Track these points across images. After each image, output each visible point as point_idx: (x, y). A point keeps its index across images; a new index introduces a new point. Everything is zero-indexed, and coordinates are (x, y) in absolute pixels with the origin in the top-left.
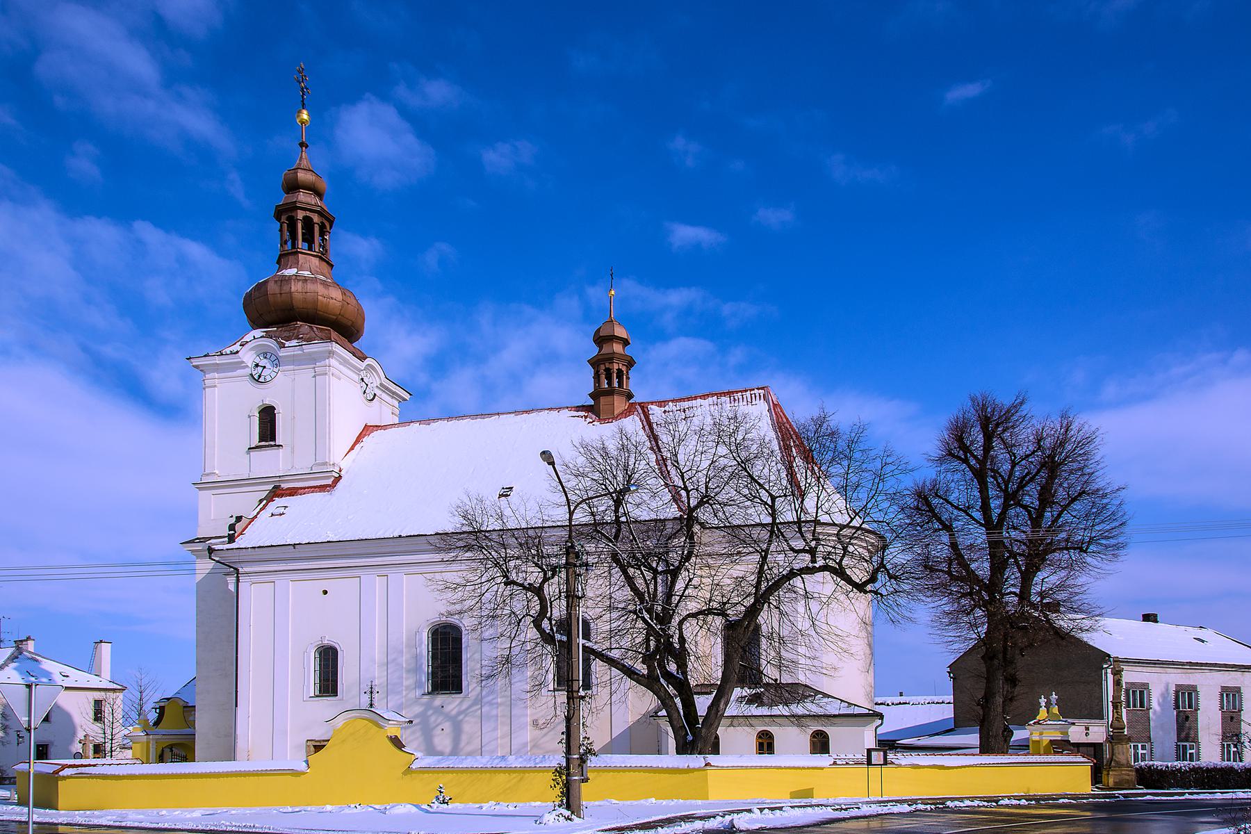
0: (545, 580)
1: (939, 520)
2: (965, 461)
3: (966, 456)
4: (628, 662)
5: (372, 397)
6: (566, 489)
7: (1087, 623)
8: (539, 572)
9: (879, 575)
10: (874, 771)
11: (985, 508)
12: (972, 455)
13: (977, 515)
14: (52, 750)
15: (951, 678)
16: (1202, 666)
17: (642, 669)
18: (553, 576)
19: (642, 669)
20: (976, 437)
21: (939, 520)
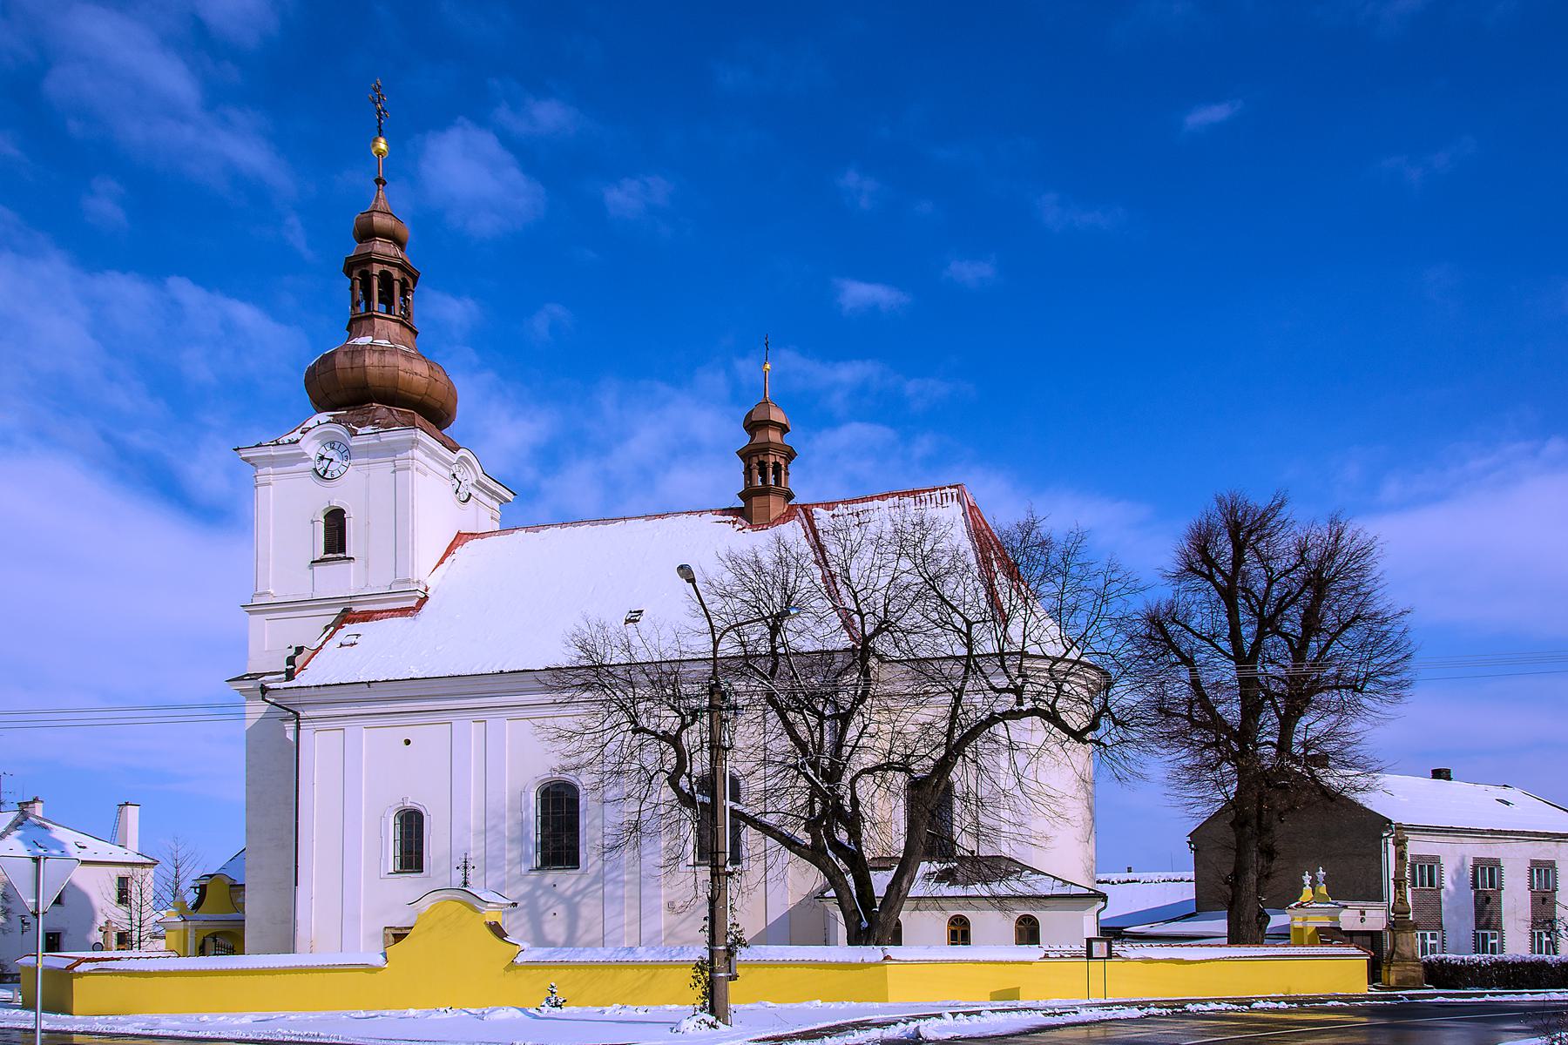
0: (684, 726)
1: (1177, 651)
3: (1211, 572)
4: (787, 830)
5: (466, 497)
6: (710, 613)
8: (676, 717)
11: (1235, 637)
12: (1219, 570)
14: (65, 940)
15: (1192, 849)
17: (805, 838)
18: (693, 722)
19: (805, 838)
20: (1224, 548)
21: (1177, 651)
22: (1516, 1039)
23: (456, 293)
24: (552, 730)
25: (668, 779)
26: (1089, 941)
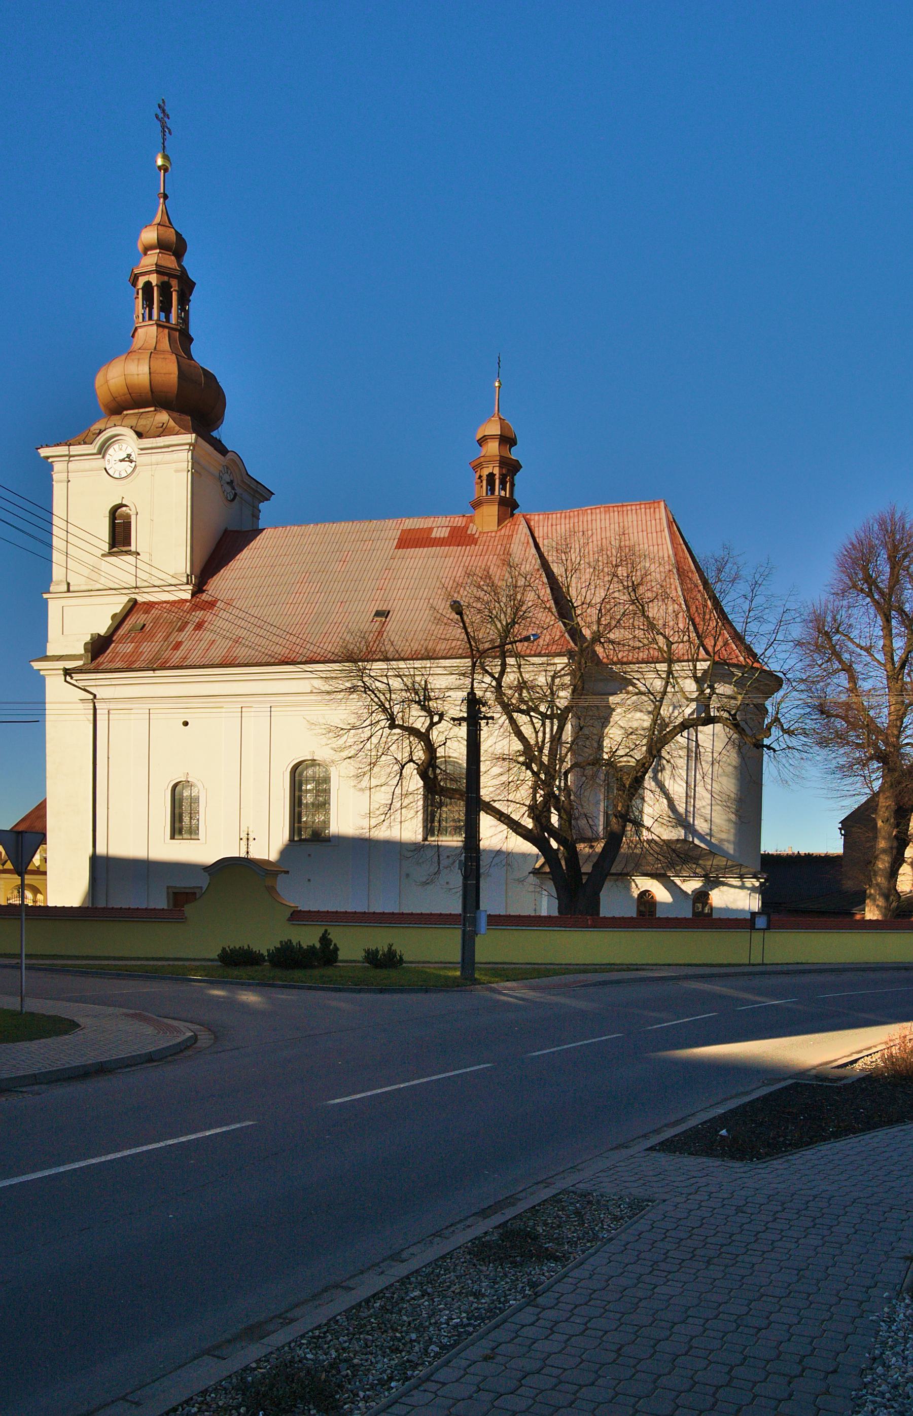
0: (432, 724)
1: (840, 661)
2: (870, 594)
3: (870, 590)
4: (516, 817)
5: (232, 497)
6: (461, 625)
7: (381, 953)
8: (426, 717)
9: (773, 729)
10: (757, 936)
11: (889, 651)
12: (877, 587)
13: (880, 657)
14: (288, 915)
15: (842, 835)
16: (63, 966)
17: (529, 823)
18: (439, 722)
19: (529, 823)
20: (883, 569)
21: (840, 661)
22: (108, 629)
23: (870, 920)
24: (324, 727)
25: (417, 769)
26: (486, 911)
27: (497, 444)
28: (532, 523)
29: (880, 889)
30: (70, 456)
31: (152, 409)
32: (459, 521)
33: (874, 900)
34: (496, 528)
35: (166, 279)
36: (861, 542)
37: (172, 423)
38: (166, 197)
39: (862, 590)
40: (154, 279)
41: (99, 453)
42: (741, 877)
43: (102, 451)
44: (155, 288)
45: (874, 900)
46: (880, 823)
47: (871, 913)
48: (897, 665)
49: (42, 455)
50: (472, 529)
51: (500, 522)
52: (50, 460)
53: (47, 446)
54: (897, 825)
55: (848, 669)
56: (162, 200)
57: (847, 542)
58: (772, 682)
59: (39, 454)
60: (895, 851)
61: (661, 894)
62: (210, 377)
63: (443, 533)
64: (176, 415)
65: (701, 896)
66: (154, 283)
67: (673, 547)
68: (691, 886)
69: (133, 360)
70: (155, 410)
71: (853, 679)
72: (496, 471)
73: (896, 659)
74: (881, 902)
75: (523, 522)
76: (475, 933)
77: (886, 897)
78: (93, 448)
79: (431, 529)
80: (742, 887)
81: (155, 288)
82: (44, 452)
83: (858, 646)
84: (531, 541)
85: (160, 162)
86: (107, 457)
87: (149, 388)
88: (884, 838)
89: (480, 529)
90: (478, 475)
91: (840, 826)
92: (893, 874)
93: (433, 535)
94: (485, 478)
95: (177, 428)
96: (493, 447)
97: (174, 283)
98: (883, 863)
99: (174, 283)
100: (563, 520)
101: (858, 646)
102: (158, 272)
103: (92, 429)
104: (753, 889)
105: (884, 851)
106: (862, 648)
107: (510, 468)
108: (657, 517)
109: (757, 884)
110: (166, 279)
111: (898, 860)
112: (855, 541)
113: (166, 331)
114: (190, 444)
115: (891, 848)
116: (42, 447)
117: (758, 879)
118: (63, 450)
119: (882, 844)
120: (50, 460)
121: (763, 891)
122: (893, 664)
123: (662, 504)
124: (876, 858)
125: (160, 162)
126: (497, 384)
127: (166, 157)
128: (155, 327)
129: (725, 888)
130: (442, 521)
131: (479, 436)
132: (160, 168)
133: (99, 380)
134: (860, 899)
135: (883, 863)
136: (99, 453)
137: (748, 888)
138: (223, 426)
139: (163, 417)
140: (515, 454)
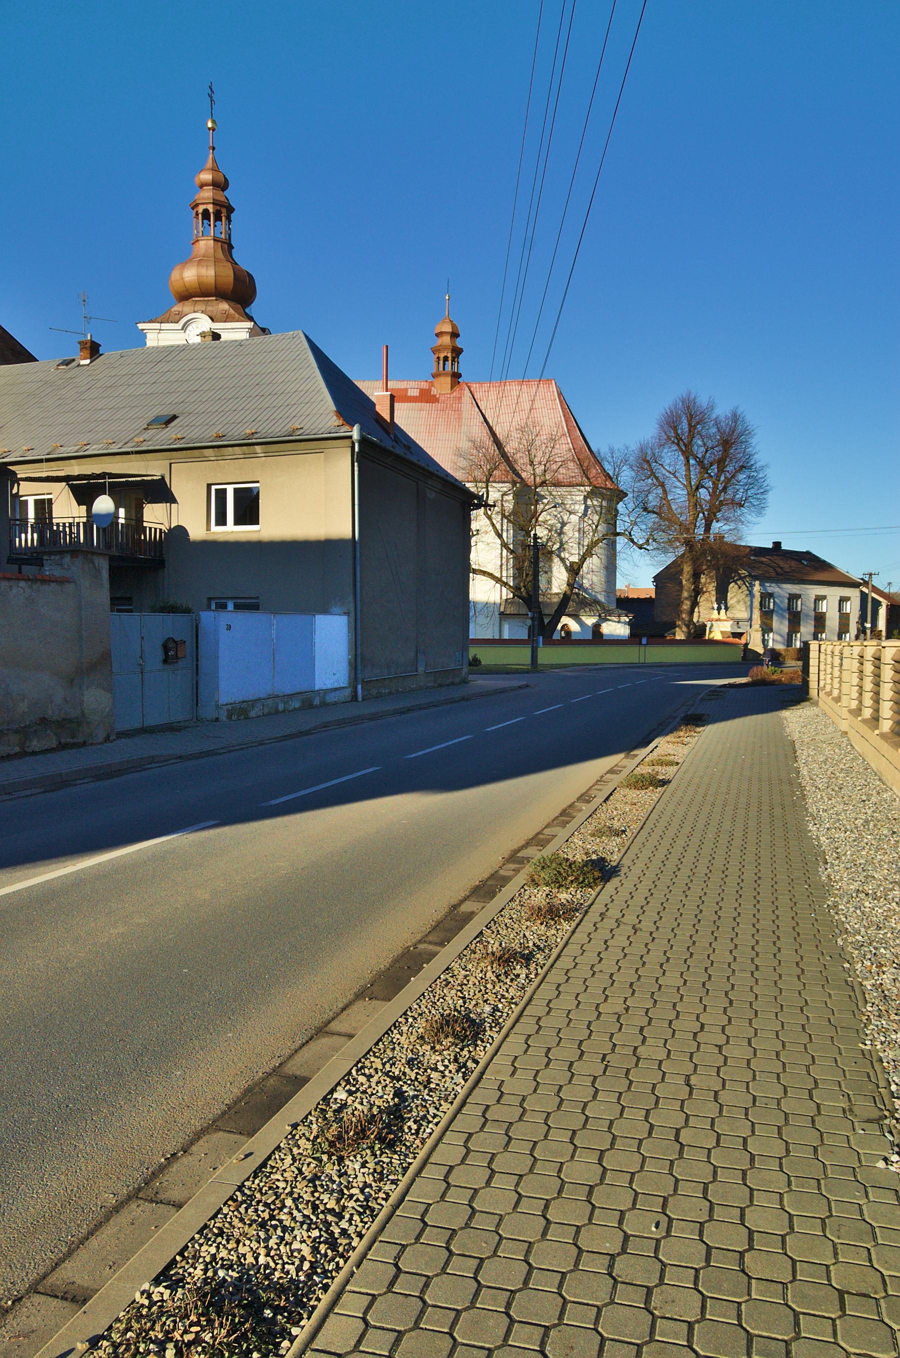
10: (642, 648)
11: (688, 478)
27: (449, 338)
28: (472, 389)
29: (685, 621)
30: (160, 330)
31: (214, 298)
32: (425, 385)
33: (681, 628)
34: (450, 392)
35: (218, 208)
36: (671, 412)
37: (232, 311)
38: (214, 149)
39: (673, 442)
40: (211, 208)
41: (182, 329)
42: (619, 616)
43: (184, 328)
44: (212, 215)
45: (681, 628)
46: (684, 582)
47: (680, 635)
48: (694, 487)
49: (140, 328)
50: (434, 391)
51: (452, 388)
52: (145, 331)
53: (144, 322)
54: (694, 583)
55: (662, 485)
56: (211, 151)
57: (664, 412)
58: (621, 495)
59: (137, 327)
60: (693, 598)
61: (574, 626)
62: (250, 276)
63: (415, 393)
64: (233, 304)
65: (597, 626)
66: (211, 210)
67: (563, 411)
68: (590, 621)
69: (203, 266)
70: (216, 300)
71: (665, 491)
72: (449, 355)
73: (693, 483)
74: (685, 629)
75: (467, 388)
76: (537, 647)
77: (688, 626)
78: (179, 326)
79: (406, 390)
80: (619, 622)
81: (212, 215)
82: (141, 326)
83: (668, 471)
84: (474, 402)
85: (210, 125)
86: (187, 331)
87: (214, 285)
88: (686, 591)
89: (439, 391)
90: (436, 356)
91: (653, 580)
92: (691, 612)
93: (409, 394)
94: (442, 359)
95: (237, 316)
96: (446, 340)
97: (224, 211)
98: (686, 605)
99: (224, 211)
100: (492, 389)
101: (668, 471)
102: (213, 204)
103: (173, 310)
104: (625, 623)
105: (687, 599)
106: (670, 473)
107: (457, 352)
108: (551, 390)
109: (628, 620)
110: (218, 208)
111: (695, 604)
112: (668, 411)
113: (220, 244)
114: (249, 329)
115: (691, 596)
116: (140, 322)
117: (628, 617)
118: (156, 326)
119: (685, 594)
120: (145, 331)
121: (630, 624)
122: (691, 487)
123: (553, 382)
124: (683, 602)
125: (210, 125)
126: (447, 298)
127: (214, 122)
128: (212, 241)
129: (610, 622)
130: (412, 384)
131: (437, 331)
132: (209, 129)
133: (175, 275)
134: (673, 626)
135: (686, 605)
136: (182, 329)
137: (622, 623)
138: (252, 305)
139: (224, 306)
140: (459, 343)
